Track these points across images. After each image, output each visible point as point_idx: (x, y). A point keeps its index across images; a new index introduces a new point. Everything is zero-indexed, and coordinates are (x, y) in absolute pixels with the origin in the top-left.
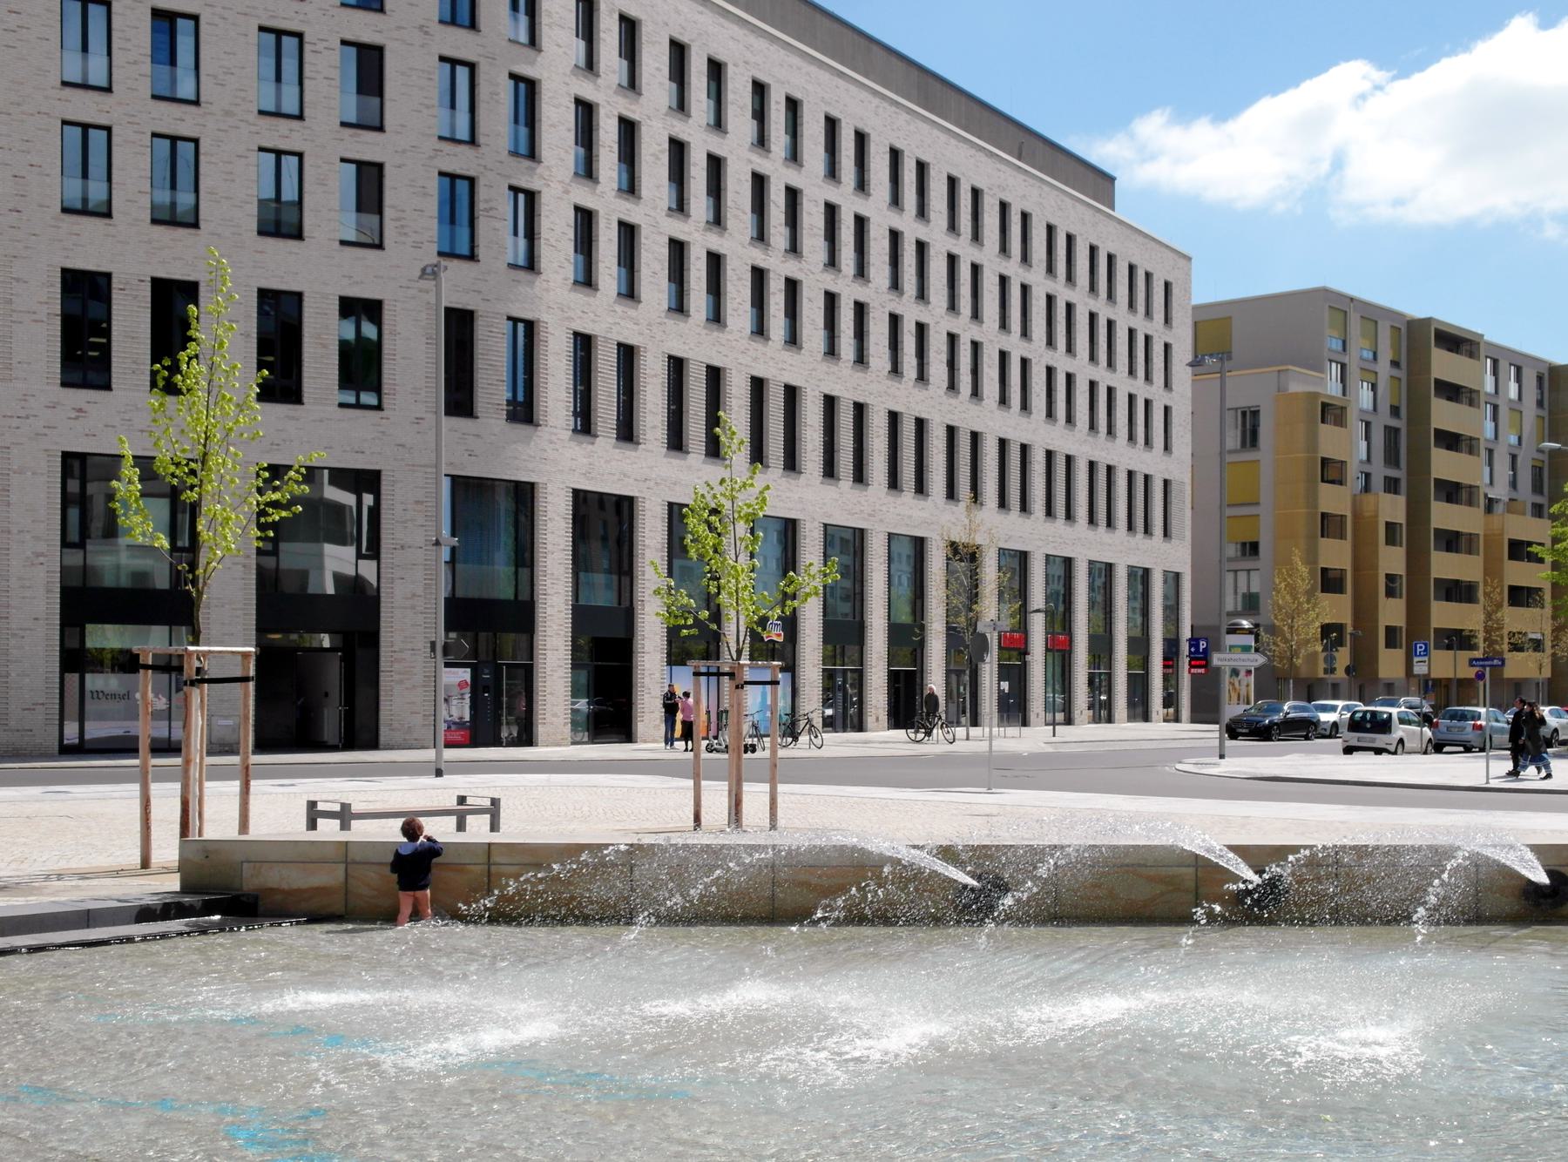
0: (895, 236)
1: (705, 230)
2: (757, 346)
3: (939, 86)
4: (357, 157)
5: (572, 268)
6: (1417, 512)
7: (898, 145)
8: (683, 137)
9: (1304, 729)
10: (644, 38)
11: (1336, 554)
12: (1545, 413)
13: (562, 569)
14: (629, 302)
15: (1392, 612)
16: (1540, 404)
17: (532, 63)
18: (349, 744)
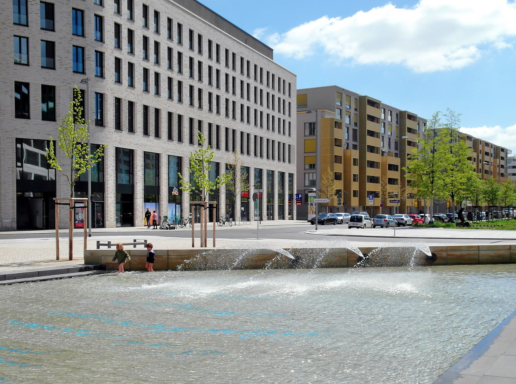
0: (210, 68)
1: (154, 65)
2: (170, 102)
3: (221, 19)
4: (46, 39)
5: (114, 77)
6: (362, 155)
7: (211, 39)
8: (147, 36)
9: (333, 221)
10: (135, 4)
11: (339, 168)
12: (398, 126)
13: (112, 172)
14: (132, 88)
15: (355, 186)
16: (397, 122)
17: (102, 11)
18: (47, 228)
